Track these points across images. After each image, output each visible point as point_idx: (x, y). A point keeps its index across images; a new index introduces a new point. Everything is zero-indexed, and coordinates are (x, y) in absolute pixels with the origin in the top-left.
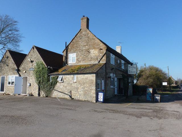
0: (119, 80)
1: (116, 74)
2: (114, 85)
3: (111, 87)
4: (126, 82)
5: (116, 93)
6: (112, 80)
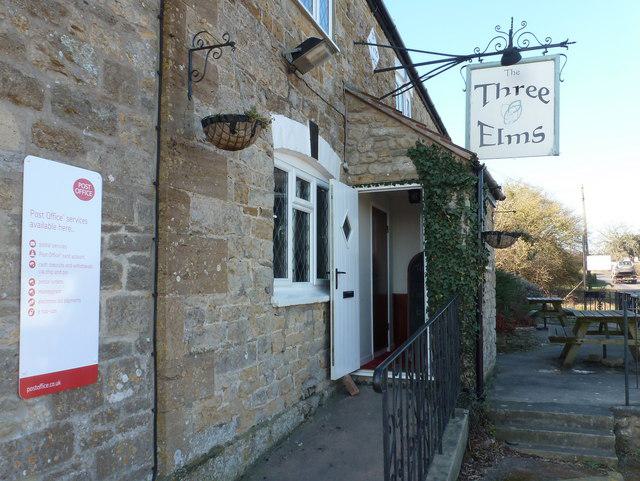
0: (382, 213)
1: (344, 148)
2: (322, 272)
3: (288, 291)
4: (465, 228)
5: (347, 360)
6: (301, 217)
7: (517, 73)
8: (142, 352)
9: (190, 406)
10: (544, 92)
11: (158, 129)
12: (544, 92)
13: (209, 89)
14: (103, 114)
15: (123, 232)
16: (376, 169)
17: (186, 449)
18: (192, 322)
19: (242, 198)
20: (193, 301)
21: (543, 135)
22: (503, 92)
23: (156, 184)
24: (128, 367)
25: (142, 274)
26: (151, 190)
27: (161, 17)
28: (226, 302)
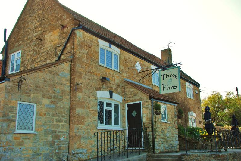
7: (170, 71)
8: (67, 133)
9: (75, 143)
10: (176, 76)
11: (70, 98)
12: (176, 76)
13: (80, 90)
14: (60, 98)
15: (64, 114)
16: (131, 99)
17: (74, 150)
18: (76, 129)
19: (89, 108)
20: (76, 126)
21: (176, 87)
22: (167, 76)
23: (70, 107)
24: (64, 135)
25: (67, 121)
26: (69, 108)
27: (70, 81)
28: (84, 127)
